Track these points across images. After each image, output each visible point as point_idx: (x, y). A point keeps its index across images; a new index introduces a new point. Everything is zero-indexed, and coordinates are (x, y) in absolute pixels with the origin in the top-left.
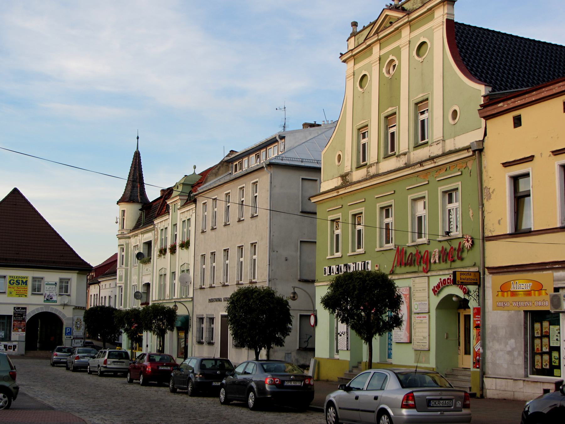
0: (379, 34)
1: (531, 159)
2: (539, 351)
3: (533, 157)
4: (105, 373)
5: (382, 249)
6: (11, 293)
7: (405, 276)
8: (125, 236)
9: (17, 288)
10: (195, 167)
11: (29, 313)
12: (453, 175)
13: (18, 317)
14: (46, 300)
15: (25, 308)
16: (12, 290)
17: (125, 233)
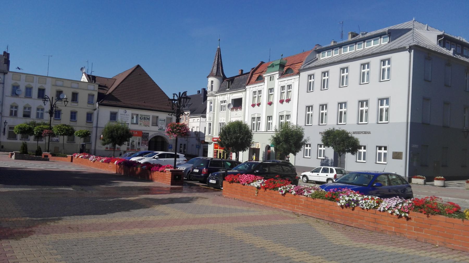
2: (224, 159)
4: (200, 186)
6: (141, 124)
8: (214, 95)
9: (144, 121)
10: (282, 56)
11: (150, 136)
13: (145, 138)
14: (159, 129)
15: (148, 133)
16: (142, 122)
17: (213, 93)
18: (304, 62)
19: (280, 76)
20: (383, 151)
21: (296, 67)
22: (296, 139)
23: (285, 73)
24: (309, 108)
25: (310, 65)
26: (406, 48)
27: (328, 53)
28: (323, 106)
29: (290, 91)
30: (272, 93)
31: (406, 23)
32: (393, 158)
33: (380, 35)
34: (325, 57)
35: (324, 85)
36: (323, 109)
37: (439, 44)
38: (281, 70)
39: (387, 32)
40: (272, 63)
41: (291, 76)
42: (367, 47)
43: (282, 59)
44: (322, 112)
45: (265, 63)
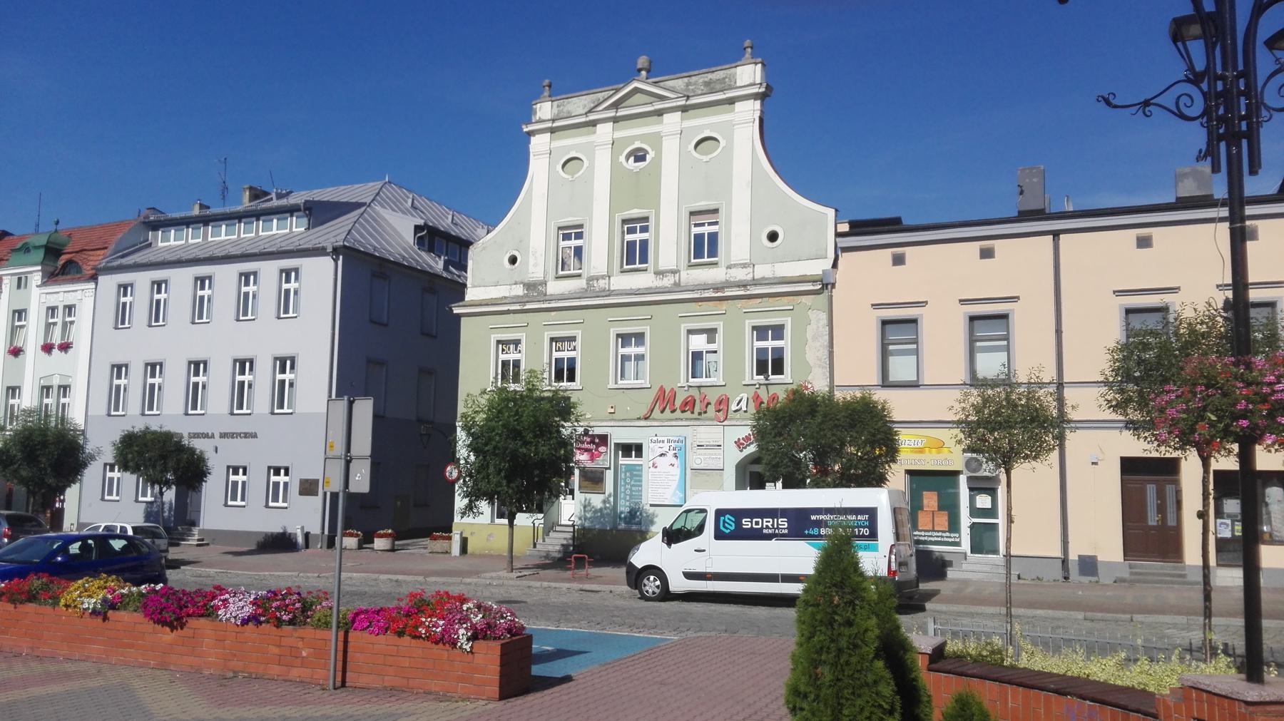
0: (619, 110)
1: (1014, 299)
3: (1179, 288)
5: (616, 386)
7: (666, 424)
10: (57, 223)
12: (632, 318)
18: (112, 247)
19: (45, 280)
20: (282, 478)
21: (91, 258)
22: (56, 453)
23: (59, 272)
24: (119, 369)
25: (125, 261)
26: (326, 249)
27: (279, 222)
28: (153, 367)
29: (22, 327)
30: (22, 323)
31: (315, 191)
32: (301, 494)
33: (291, 210)
34: (169, 242)
35: (156, 312)
36: (197, 374)
37: (418, 244)
38: (51, 263)
39: (302, 205)
40: (24, 241)
41: (73, 281)
42: (264, 234)
43: (56, 231)
44: (193, 379)
45: (12, 235)
